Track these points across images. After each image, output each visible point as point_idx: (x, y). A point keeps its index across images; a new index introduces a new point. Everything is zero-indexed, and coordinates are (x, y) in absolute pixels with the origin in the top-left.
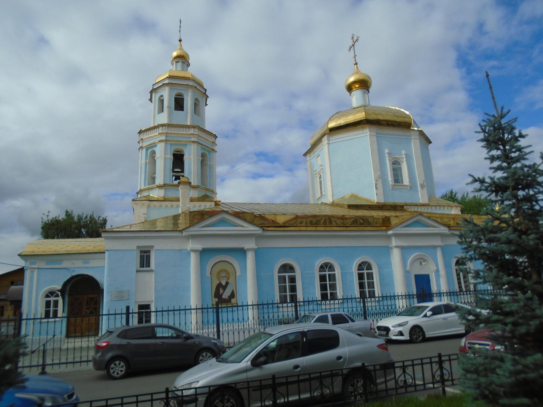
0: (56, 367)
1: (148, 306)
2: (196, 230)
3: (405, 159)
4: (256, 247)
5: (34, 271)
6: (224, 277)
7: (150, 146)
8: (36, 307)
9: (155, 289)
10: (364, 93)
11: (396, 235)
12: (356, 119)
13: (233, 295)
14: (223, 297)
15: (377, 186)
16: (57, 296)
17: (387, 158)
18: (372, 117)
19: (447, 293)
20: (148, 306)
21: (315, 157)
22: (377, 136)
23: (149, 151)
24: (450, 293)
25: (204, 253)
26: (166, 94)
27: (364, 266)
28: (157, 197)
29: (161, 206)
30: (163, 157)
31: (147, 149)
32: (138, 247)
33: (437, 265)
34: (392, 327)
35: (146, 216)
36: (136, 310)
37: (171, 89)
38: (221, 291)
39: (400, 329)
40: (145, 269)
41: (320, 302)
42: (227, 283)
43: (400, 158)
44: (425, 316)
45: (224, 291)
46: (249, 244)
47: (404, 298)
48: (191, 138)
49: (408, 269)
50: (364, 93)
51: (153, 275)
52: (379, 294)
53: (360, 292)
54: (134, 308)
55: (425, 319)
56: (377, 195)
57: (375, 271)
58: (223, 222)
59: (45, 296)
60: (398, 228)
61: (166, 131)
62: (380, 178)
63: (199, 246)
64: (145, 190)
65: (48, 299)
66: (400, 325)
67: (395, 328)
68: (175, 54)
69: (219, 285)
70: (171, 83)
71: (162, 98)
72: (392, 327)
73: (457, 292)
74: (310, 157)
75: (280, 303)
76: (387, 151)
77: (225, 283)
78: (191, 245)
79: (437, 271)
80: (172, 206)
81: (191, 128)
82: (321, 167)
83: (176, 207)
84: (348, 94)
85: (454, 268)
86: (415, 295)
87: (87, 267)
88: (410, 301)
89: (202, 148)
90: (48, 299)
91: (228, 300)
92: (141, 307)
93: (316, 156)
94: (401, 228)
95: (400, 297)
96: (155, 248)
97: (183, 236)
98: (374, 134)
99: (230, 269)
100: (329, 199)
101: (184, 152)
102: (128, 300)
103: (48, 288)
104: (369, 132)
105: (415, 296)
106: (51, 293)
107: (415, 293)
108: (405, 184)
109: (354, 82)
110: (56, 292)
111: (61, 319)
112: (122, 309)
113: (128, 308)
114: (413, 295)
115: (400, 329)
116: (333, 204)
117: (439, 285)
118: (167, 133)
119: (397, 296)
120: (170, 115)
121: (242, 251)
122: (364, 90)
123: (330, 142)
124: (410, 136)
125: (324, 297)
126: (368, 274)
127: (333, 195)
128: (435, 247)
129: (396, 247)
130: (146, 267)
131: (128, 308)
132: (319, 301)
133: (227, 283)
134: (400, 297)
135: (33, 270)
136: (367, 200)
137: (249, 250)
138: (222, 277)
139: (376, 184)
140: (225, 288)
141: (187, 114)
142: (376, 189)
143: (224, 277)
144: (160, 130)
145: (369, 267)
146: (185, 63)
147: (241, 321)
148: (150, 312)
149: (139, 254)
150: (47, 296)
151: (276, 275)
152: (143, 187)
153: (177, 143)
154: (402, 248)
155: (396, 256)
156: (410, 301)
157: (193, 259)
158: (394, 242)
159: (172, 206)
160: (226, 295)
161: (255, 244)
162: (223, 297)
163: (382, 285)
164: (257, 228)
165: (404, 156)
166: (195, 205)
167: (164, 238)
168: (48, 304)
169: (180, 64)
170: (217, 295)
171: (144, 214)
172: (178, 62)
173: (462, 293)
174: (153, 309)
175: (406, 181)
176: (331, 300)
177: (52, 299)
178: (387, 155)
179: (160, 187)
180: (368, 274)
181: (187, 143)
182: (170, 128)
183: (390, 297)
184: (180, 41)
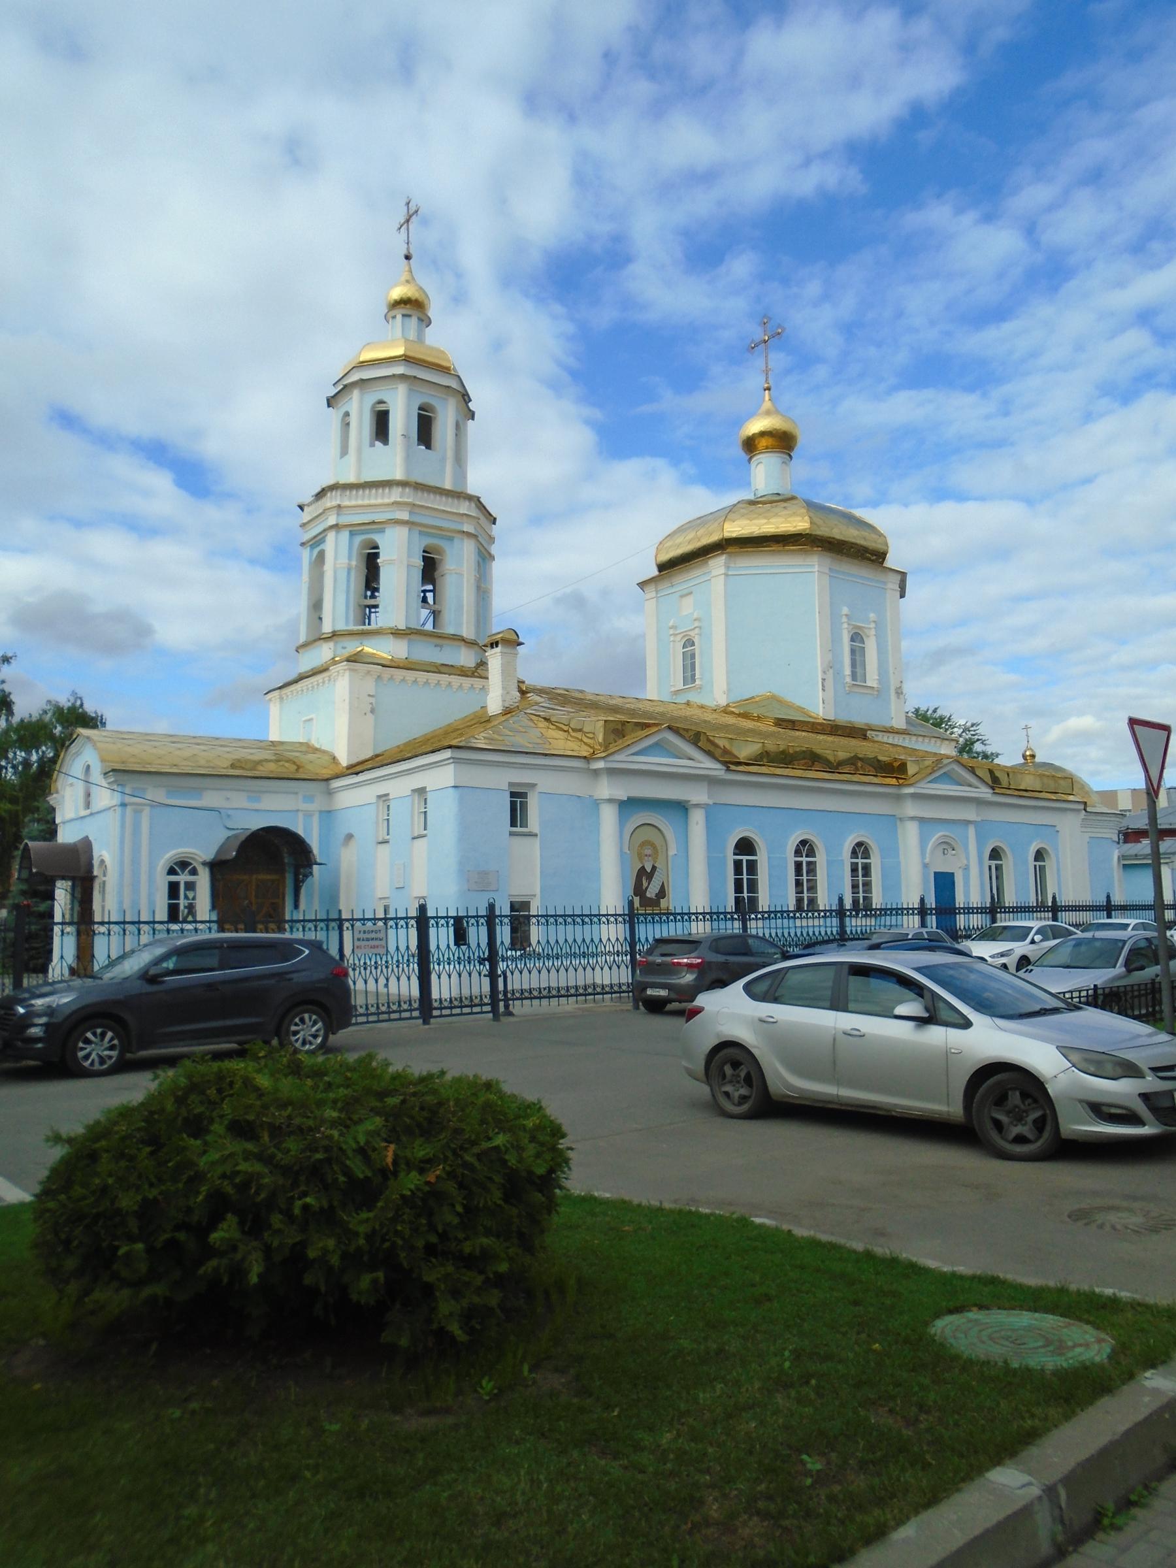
0: (554, 1001)
1: (526, 905)
2: (622, 760)
3: (873, 632)
4: (711, 802)
5: (141, 811)
6: (650, 856)
7: (363, 528)
8: (150, 896)
9: (541, 872)
10: (783, 462)
11: (915, 796)
12: (789, 531)
13: (662, 893)
14: (648, 895)
15: (825, 685)
16: (194, 872)
17: (845, 626)
18: (823, 531)
19: (704, 914)
20: (526, 905)
21: (677, 595)
22: (726, 575)
23: (358, 539)
24: (711, 913)
25: (628, 805)
26: (359, 407)
27: (861, 849)
28: (390, 657)
29: (438, 683)
30: (405, 563)
31: (352, 534)
32: (511, 784)
33: (968, 859)
34: (990, 957)
35: (372, 700)
36: (506, 911)
37: (410, 389)
38: (645, 884)
39: (1003, 960)
40: (518, 829)
41: (792, 915)
42: (654, 868)
43: (867, 628)
44: (1033, 942)
45: (649, 884)
46: (697, 795)
47: (442, 925)
48: (463, 523)
49: (927, 860)
50: (783, 462)
51: (536, 843)
52: (63, 916)
53: (736, 898)
54: (503, 908)
55: (1033, 947)
56: (823, 703)
57: (875, 862)
58: (659, 748)
59: (167, 871)
60: (922, 784)
61: (338, 502)
62: (831, 667)
63: (622, 791)
64: (351, 634)
65: (174, 878)
66: (1002, 955)
67: (993, 960)
68: (397, 293)
69: (642, 871)
70: (415, 377)
71: (382, 407)
72: (990, 957)
73: (1033, 907)
74: (657, 592)
75: (735, 913)
76: (845, 610)
77: (651, 867)
78: (605, 789)
79: (966, 868)
80: (391, 678)
81: (462, 500)
82: (696, 624)
83: (457, 690)
84: (746, 457)
85: (987, 862)
86: (412, 918)
87: (257, 810)
88: (62, 940)
89: (421, 533)
90: (174, 878)
91: (655, 902)
92: (513, 907)
93: (680, 593)
94: (633, 754)
95: (402, 923)
96: (539, 789)
97: (588, 769)
98: (827, 571)
99: (658, 842)
100: (722, 701)
101: (377, 547)
102: (497, 891)
103: (168, 856)
104: (819, 565)
105: (482, 920)
106: (183, 864)
107: (934, 906)
108: (869, 684)
109: (763, 434)
110: (191, 864)
111: (208, 924)
112: (407, 909)
113: (491, 907)
114: (913, 909)
115: (1003, 960)
116: (726, 711)
117: (967, 894)
118: (339, 506)
119: (433, 918)
120: (408, 458)
121: (681, 808)
122: (782, 455)
123: (730, 573)
124: (885, 583)
125: (799, 907)
126: (809, 863)
127: (729, 691)
128: (968, 822)
129: (912, 818)
130: (521, 827)
131: (491, 907)
132: (791, 911)
133: (654, 868)
134: (779, 915)
135: (140, 807)
136: (801, 709)
137: (697, 806)
138: (646, 855)
139: (824, 680)
140: (650, 876)
141: (443, 460)
142: (823, 690)
143: (650, 856)
144: (396, 495)
145: (811, 853)
146: (422, 321)
147: (392, 954)
148: (528, 917)
149: (508, 799)
150: (172, 871)
151: (731, 858)
152: (341, 626)
153: (439, 532)
154: (921, 820)
155: (910, 834)
156: (62, 940)
157: (609, 815)
158: (911, 809)
159: (427, 683)
160: (652, 892)
161: (707, 797)
162: (648, 895)
163: (885, 888)
164: (719, 766)
165: (873, 625)
166: (472, 685)
167: (497, 766)
168: (173, 889)
169: (413, 322)
170: (639, 890)
171: (369, 695)
172: (409, 316)
173: (753, 916)
174: (533, 912)
175: (872, 680)
176: (808, 911)
177: (182, 878)
178: (844, 619)
179: (396, 633)
180: (809, 863)
181: (454, 535)
182: (420, 493)
183: (682, 914)
184: (408, 257)
